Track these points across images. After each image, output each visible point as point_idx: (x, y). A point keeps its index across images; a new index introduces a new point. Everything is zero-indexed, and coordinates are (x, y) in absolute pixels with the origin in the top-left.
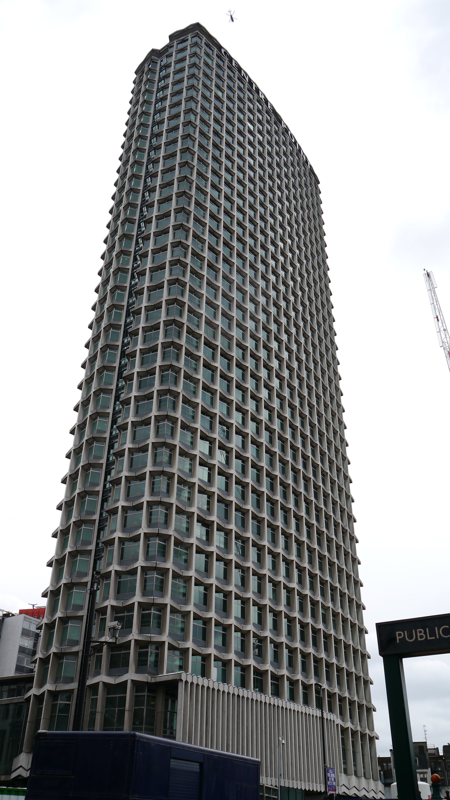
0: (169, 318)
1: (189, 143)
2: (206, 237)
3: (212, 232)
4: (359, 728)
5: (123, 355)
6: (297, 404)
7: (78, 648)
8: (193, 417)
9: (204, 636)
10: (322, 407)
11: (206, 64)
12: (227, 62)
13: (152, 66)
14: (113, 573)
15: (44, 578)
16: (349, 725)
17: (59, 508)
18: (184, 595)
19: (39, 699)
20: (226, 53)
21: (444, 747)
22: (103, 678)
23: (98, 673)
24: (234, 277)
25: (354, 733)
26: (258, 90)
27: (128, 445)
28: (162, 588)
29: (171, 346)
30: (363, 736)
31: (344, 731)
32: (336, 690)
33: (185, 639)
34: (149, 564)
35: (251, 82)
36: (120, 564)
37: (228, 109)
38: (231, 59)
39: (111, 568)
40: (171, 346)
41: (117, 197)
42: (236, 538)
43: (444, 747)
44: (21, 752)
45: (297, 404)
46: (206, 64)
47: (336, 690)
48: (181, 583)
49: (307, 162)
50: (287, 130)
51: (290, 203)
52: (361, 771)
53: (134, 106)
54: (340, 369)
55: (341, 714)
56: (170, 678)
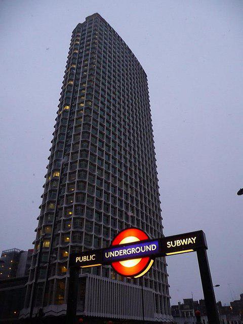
0: (81, 169)
1: (92, 72)
2: (100, 98)
3: (102, 90)
4: (163, 294)
5: (67, 137)
6: (137, 157)
7: (46, 265)
8: (94, 170)
9: (99, 231)
10: (147, 159)
11: (100, 29)
12: (109, 29)
13: (79, 32)
14: (55, 280)
15: (33, 236)
16: (159, 293)
17: (40, 208)
18: (91, 215)
19: (31, 286)
20: (108, 25)
21: (200, 300)
22: (56, 277)
23: (54, 275)
24: (112, 114)
25: (161, 296)
26: (121, 40)
27: (67, 182)
28: (83, 200)
29: (85, 151)
30: (165, 297)
31: (156, 295)
32: (153, 279)
33: (91, 231)
34: (75, 230)
35: (119, 37)
36: (64, 230)
37: (109, 47)
38: (111, 28)
39: (58, 246)
40: (85, 151)
41: (65, 83)
42: (112, 186)
43: (200, 300)
44: (23, 308)
45: (137, 157)
46: (100, 29)
47: (153, 279)
48: (90, 211)
49: (142, 68)
50: (134, 55)
51: (134, 75)
52: (163, 310)
53: (71, 46)
54: (157, 163)
55: (155, 288)
56: (83, 276)
